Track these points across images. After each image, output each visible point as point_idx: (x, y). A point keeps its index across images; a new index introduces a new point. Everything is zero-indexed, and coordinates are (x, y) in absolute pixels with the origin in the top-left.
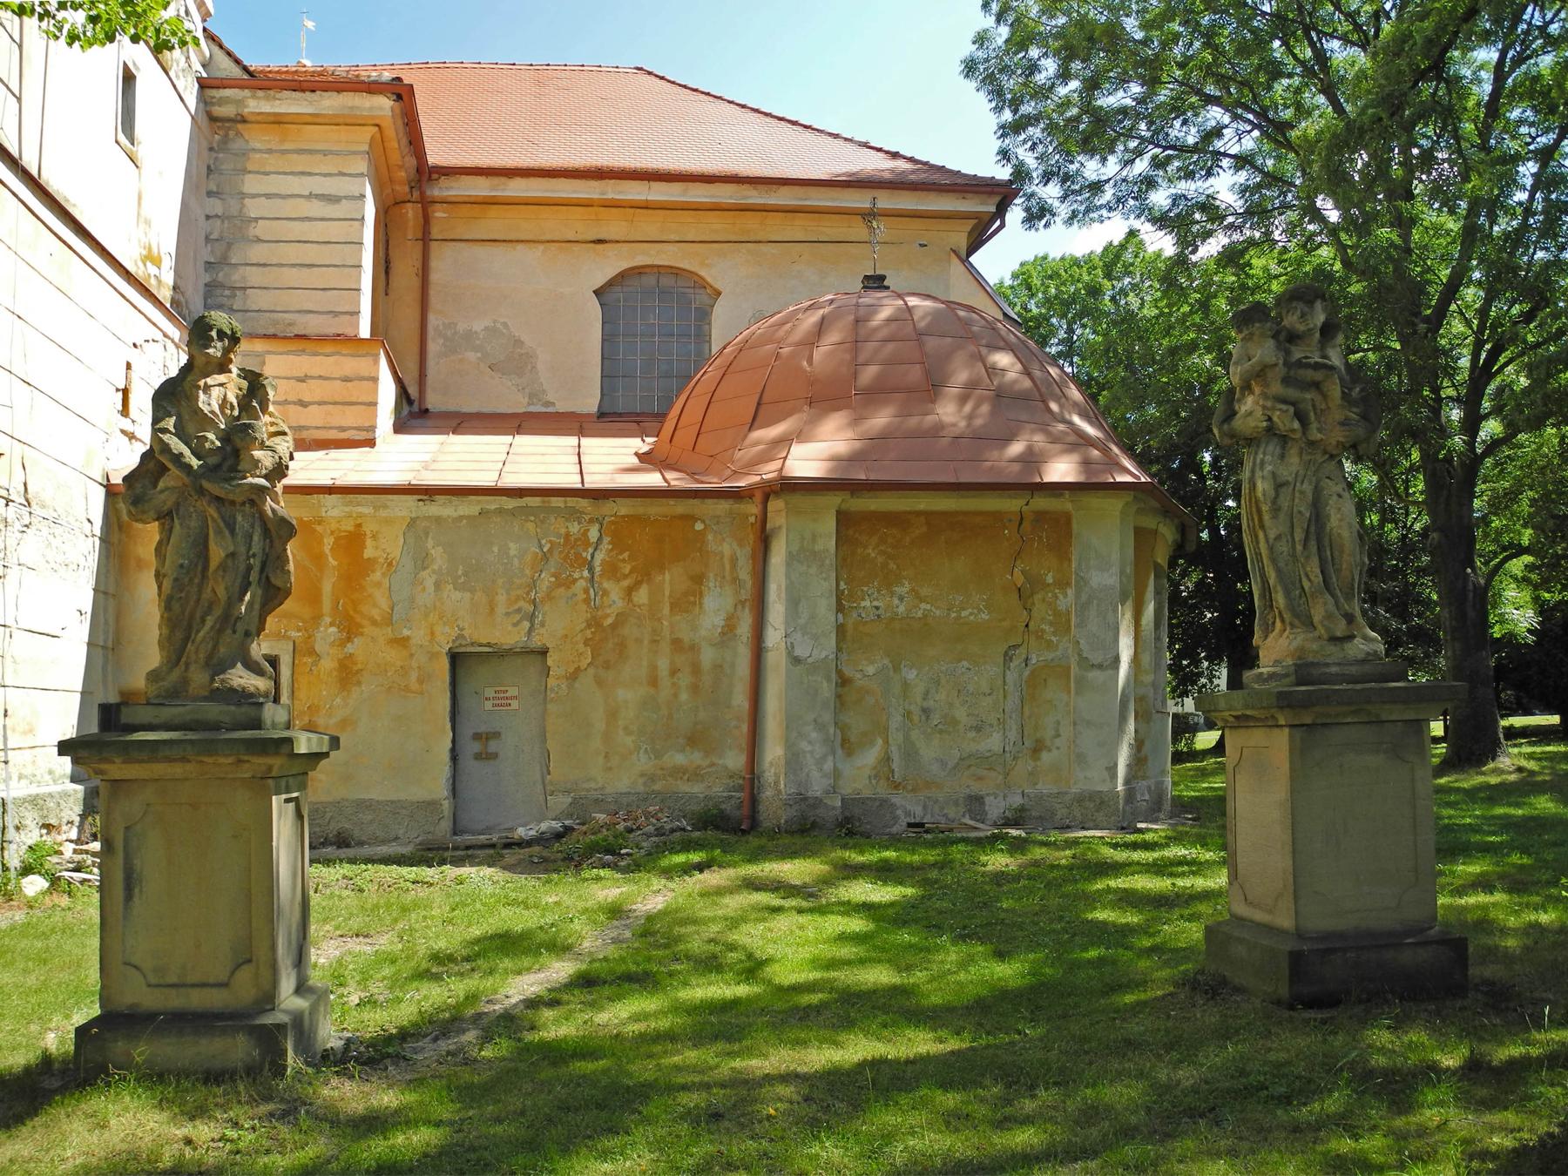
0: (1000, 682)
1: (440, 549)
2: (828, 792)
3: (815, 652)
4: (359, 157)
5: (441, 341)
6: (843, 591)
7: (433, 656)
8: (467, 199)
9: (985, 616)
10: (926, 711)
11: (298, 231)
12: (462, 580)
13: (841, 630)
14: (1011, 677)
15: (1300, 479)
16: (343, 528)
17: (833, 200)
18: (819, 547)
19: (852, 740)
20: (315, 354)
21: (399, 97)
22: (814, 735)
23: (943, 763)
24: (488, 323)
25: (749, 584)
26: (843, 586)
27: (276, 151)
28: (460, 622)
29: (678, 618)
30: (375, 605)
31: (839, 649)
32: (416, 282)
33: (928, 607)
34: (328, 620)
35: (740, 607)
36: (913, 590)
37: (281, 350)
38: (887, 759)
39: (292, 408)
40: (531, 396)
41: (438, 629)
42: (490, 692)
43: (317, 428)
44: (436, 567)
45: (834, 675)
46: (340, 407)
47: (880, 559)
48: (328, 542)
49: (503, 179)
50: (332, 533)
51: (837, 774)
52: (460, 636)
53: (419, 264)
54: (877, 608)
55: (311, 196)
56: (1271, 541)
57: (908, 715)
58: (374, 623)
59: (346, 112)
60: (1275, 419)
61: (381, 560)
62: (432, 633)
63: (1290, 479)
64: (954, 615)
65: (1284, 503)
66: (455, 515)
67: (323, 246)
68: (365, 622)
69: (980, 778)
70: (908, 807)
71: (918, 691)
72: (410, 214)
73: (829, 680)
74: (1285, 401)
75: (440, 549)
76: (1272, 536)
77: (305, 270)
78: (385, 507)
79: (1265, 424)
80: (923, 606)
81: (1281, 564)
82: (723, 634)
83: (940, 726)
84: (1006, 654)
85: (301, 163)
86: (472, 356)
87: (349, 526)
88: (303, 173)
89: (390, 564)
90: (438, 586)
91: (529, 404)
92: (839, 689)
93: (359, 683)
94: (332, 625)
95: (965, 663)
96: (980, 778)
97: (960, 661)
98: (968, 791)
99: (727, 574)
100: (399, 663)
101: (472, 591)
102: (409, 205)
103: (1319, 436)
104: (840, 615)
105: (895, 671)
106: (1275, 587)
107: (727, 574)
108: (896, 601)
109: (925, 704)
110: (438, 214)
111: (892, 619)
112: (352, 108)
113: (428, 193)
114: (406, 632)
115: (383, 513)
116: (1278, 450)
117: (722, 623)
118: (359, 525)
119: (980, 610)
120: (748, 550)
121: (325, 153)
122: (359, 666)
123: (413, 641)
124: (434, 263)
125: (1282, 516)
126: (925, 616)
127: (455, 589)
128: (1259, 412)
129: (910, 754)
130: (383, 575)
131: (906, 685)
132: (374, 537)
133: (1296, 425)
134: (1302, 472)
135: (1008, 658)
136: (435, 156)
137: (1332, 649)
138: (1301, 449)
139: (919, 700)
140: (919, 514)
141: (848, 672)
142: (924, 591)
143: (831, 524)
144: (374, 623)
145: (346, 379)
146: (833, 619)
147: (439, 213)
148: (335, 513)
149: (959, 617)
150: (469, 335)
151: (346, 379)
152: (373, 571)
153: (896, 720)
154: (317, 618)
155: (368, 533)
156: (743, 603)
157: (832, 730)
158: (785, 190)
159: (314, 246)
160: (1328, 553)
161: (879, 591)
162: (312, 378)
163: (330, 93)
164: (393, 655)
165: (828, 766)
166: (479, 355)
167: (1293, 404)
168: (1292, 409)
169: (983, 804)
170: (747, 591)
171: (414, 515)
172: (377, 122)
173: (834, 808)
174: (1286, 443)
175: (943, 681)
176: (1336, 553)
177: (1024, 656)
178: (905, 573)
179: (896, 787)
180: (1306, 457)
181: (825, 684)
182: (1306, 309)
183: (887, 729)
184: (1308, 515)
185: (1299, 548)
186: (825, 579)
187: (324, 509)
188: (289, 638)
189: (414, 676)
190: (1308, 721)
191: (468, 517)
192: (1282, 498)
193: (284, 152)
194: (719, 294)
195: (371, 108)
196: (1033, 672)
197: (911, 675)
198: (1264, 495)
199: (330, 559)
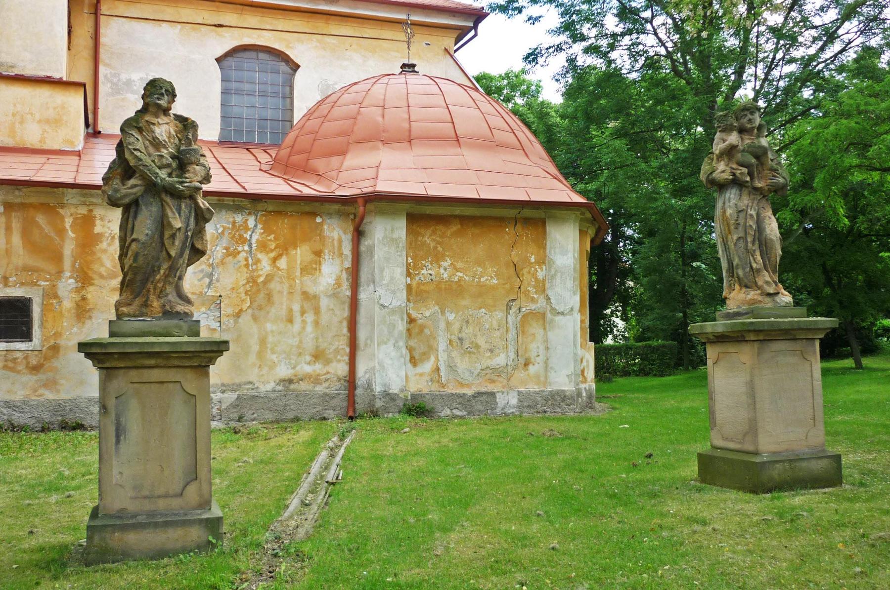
10: (460, 339)
18: (395, 236)
30: (102, 265)
32: (90, 43)
33: (461, 275)
36: (452, 264)
45: (405, 317)
47: (432, 244)
50: (71, 215)
53: (92, 30)
54: (431, 275)
61: (107, 235)
68: (95, 276)
80: (458, 274)
93: (90, 318)
94: (70, 277)
108: (442, 271)
109: (460, 336)
111: (440, 282)
124: (102, 31)
126: (459, 280)
129: (452, 368)
131: (448, 324)
152: (101, 242)
154: (60, 272)
170: (348, 264)
181: (400, 322)
186: (400, 256)
199: (70, 233)
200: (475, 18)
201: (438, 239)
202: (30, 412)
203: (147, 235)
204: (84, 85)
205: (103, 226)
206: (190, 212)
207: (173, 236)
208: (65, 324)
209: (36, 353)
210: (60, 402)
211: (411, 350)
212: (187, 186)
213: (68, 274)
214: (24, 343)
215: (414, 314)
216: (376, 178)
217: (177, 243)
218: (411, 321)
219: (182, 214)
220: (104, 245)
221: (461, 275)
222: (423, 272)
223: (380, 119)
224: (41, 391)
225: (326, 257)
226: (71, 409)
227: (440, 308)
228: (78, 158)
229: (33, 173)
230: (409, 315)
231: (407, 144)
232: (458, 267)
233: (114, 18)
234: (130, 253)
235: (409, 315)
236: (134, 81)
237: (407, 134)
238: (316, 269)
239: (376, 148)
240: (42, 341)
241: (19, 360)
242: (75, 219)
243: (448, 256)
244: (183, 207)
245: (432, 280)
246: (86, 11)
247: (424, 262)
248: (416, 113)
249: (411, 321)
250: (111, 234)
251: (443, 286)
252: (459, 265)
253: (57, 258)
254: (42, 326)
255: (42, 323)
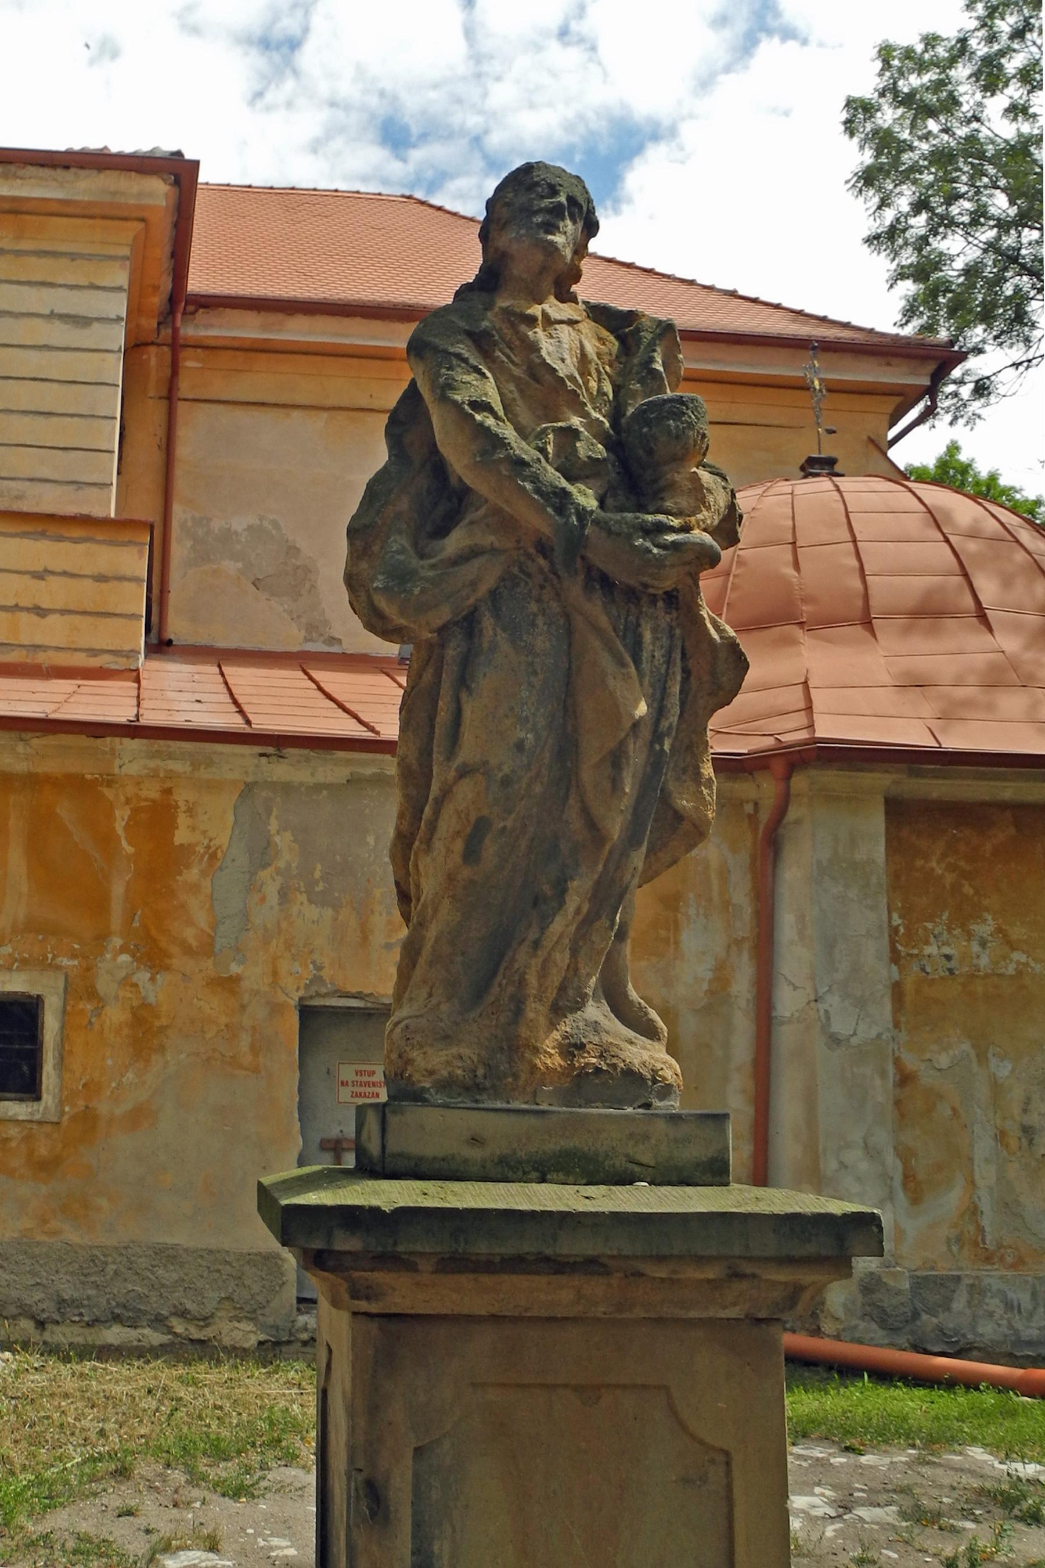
1: (288, 836)
3: (862, 1027)
4: (118, 264)
5: (189, 543)
7: (276, 1009)
8: (229, 343)
10: (1027, 1130)
11: (33, 363)
12: (320, 887)
16: (144, 793)
17: (715, 361)
18: (860, 856)
19: (921, 1176)
20: (60, 539)
21: (177, 182)
22: (864, 1166)
24: (252, 520)
25: (748, 912)
27: (9, 252)
28: (316, 956)
29: (643, 964)
30: (190, 922)
32: (157, 457)
33: (1023, 958)
34: (117, 942)
35: (734, 948)
36: (999, 930)
37: (19, 531)
38: (974, 1211)
39: (24, 616)
40: (311, 628)
41: (284, 966)
42: (347, 1073)
43: (58, 649)
44: (281, 864)
45: (891, 1069)
46: (90, 619)
47: (949, 878)
48: (121, 816)
49: (280, 316)
50: (128, 801)
52: (317, 980)
53: (161, 432)
54: (948, 958)
55: (52, 316)
57: (1001, 1136)
58: (188, 950)
59: (107, 198)
61: (201, 849)
62: (275, 973)
66: (310, 780)
67: (65, 387)
68: (174, 950)
70: (1011, 1295)
72: (153, 361)
73: (883, 1074)
75: (288, 836)
77: (41, 419)
78: (209, 763)
80: (1018, 956)
82: (711, 992)
85: (40, 267)
86: (230, 566)
87: (151, 792)
88: (43, 284)
89: (213, 856)
90: (284, 895)
91: (307, 640)
93: (162, 1049)
94: (123, 949)
99: (715, 894)
100: (224, 1020)
101: (336, 907)
102: (152, 349)
107: (715, 894)
108: (975, 948)
109: (1027, 1120)
110: (189, 364)
111: (972, 977)
112: (114, 194)
113: (182, 332)
114: (235, 969)
115: (204, 774)
117: (710, 975)
118: (168, 791)
120: (744, 858)
121: (73, 256)
122: (164, 1021)
123: (245, 984)
124: (182, 433)
126: (1019, 974)
127: (310, 901)
129: (1009, 1206)
130: (204, 873)
131: (997, 1088)
132: (190, 811)
136: (197, 283)
139: (1016, 1111)
140: (1003, 806)
142: (1017, 932)
144: (188, 950)
145: (101, 578)
147: (190, 363)
148: (133, 769)
150: (227, 536)
151: (101, 578)
152: (188, 867)
154: (102, 938)
155: (181, 804)
156: (738, 942)
159: (55, 385)
161: (949, 930)
162: (53, 573)
163: (87, 172)
164: (212, 1005)
166: (240, 565)
170: (745, 925)
171: (250, 779)
172: (140, 215)
173: (899, 1293)
178: (986, 902)
181: (878, 1082)
186: (873, 908)
187: (117, 762)
188: (58, 968)
189: (245, 1041)
191: (328, 786)
193: (19, 253)
195: (140, 195)
197: (1004, 1070)
199: (124, 843)
200: (931, 367)
201: (962, 863)
202: (33, 1273)
203: (520, 746)
204: (152, 527)
205: (193, 829)
206: (669, 661)
207: (616, 759)
208: (109, 1062)
209: (48, 1128)
210: (95, 1252)
211: (905, 1154)
212: (675, 544)
213: (117, 942)
214: (24, 1105)
215: (911, 1062)
216: (809, 708)
217: (628, 786)
218: (905, 1079)
219: (645, 666)
220: (193, 874)
221: (1023, 958)
222: (928, 950)
223: (791, 571)
224: (54, 1224)
225: (692, 911)
226: (116, 1273)
227: (973, 1046)
228: (136, 685)
229: (53, 707)
230: (897, 1062)
231: (859, 631)
232: (1014, 937)
233: (203, 405)
234: (447, 823)
235: (897, 1062)
236: (236, 532)
237: (860, 603)
238: (667, 941)
239: (790, 642)
240: (61, 1103)
241: (13, 1144)
242: (136, 811)
243: (987, 910)
244: (648, 636)
245: (951, 971)
246: (151, 394)
247: (929, 925)
248: (874, 556)
249: (905, 1079)
250: (208, 847)
251: (980, 989)
252: (1017, 932)
253: (99, 905)
254: (61, 1063)
255: (62, 1058)
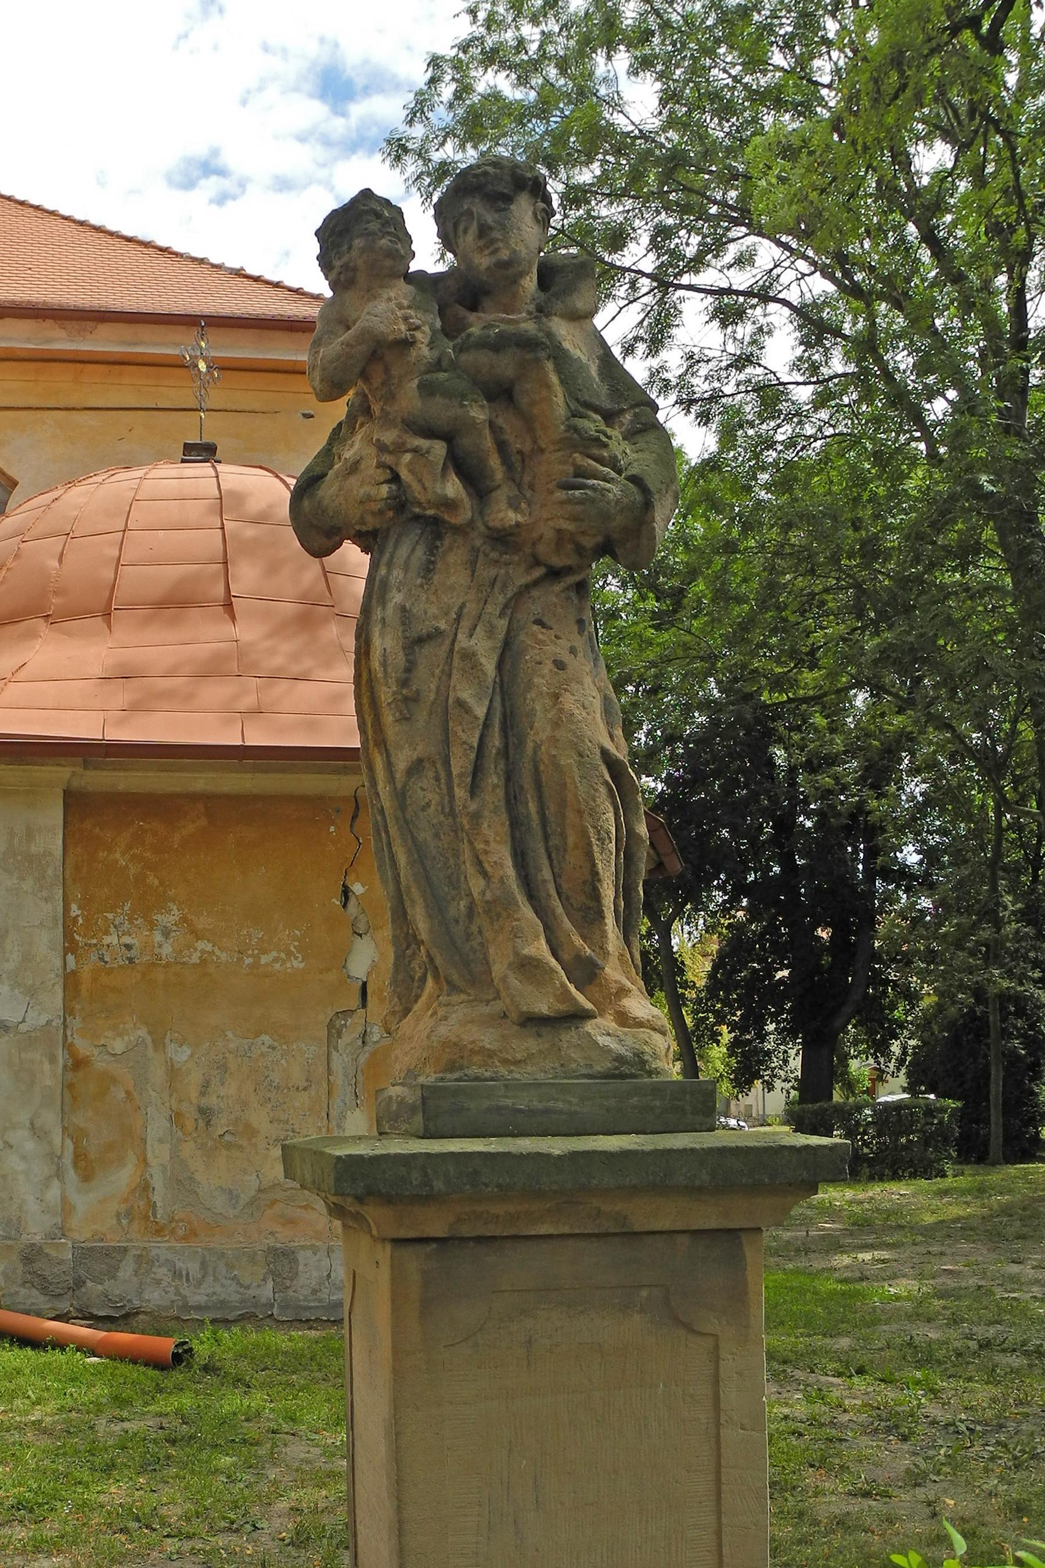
0: (321, 1069)
2: (51, 1236)
3: (31, 1014)
6: (75, 920)
9: (297, 964)
10: (206, 1114)
13: (70, 981)
14: (340, 1062)
15: (465, 624)
19: (92, 1156)
22: (30, 1145)
23: (232, 1196)
26: (75, 910)
31: (68, 1010)
33: (209, 947)
36: (184, 919)
38: (145, 1188)
47: (133, 870)
51: (67, 1208)
54: (129, 947)
56: (399, 776)
57: (176, 1118)
60: (404, 474)
63: (443, 625)
64: (248, 961)
65: (426, 682)
69: (291, 1222)
70: (179, 1265)
71: (195, 1078)
74: (429, 433)
76: (402, 761)
79: (384, 490)
80: (201, 945)
81: (425, 835)
83: (227, 1138)
84: (331, 1025)
92: (70, 1075)
95: (266, 1038)
96: (291, 1222)
97: (257, 1035)
98: (271, 1242)
103: (513, 517)
104: (70, 958)
105: (156, 1050)
106: (408, 887)
108: (158, 937)
109: (204, 1102)
116: (420, 553)
119: (289, 954)
125: (422, 716)
126: (203, 962)
128: (370, 467)
131: (173, 1072)
133: (453, 487)
134: (471, 608)
135: (334, 1031)
137: (529, 1044)
138: (475, 551)
139: (194, 1094)
140: (194, 797)
141: (83, 1046)
142: (203, 922)
143: (55, 815)
146: (58, 963)
149: (256, 965)
153: (157, 1127)
157: (57, 1139)
158: (105, 330)
160: (532, 807)
161: (131, 922)
165: (53, 1194)
167: (448, 437)
168: (439, 449)
169: (295, 1261)
173: (61, 1262)
174: (439, 536)
175: (232, 1065)
176: (552, 808)
177: (360, 1029)
179: (159, 1231)
180: (487, 573)
181: (47, 1066)
182: (490, 218)
183: (144, 1141)
184: (481, 711)
185: (460, 793)
186: (46, 900)
190: (438, 1229)
192: (422, 670)
194: (15, 484)
196: (373, 1054)
197: (182, 1055)
198: (384, 664)
